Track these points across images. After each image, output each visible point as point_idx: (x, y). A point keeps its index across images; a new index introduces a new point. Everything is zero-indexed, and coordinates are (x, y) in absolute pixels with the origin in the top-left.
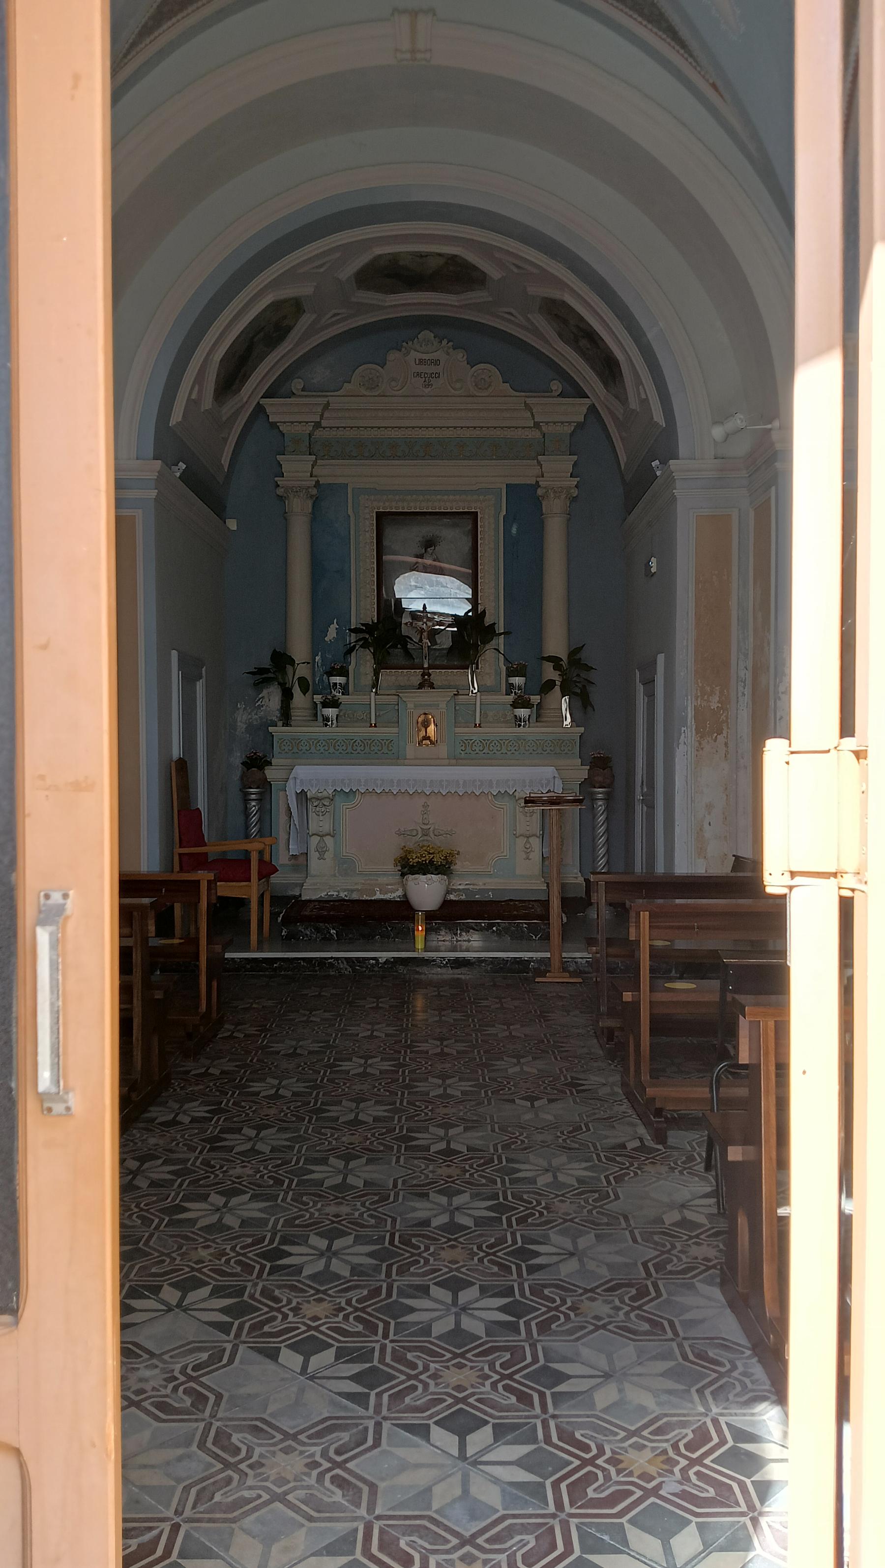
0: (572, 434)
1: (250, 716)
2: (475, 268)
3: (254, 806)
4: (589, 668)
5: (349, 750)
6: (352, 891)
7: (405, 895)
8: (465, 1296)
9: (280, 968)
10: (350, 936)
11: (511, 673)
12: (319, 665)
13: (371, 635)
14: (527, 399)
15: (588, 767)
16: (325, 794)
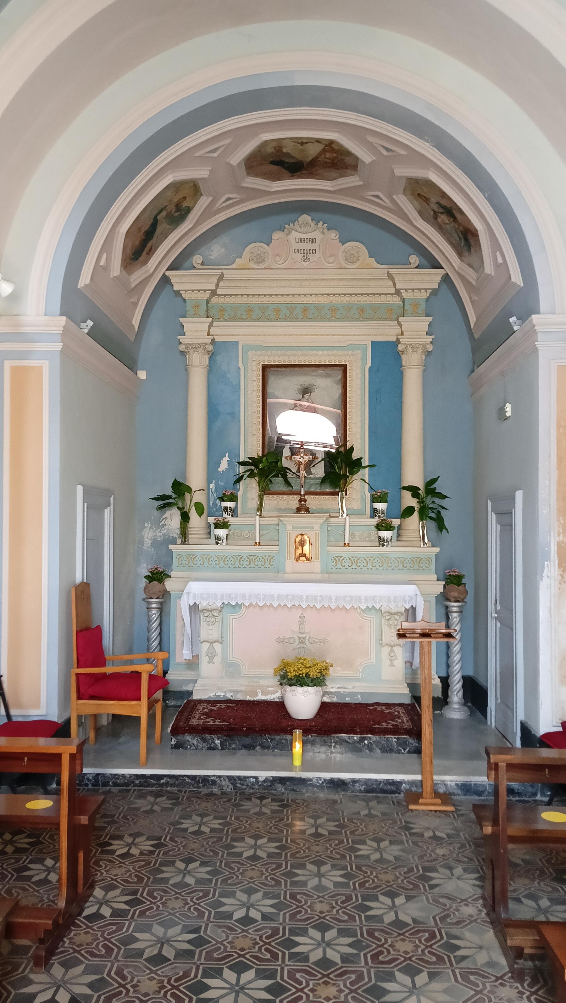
0: (427, 300)
1: (155, 534)
2: (349, 153)
3: (155, 614)
4: (444, 497)
5: (237, 564)
6: (237, 692)
7: (282, 697)
8: (324, 869)
9: (167, 784)
10: (234, 746)
11: (374, 499)
12: (213, 491)
13: (257, 467)
14: (389, 270)
15: (444, 583)
16: (214, 607)
